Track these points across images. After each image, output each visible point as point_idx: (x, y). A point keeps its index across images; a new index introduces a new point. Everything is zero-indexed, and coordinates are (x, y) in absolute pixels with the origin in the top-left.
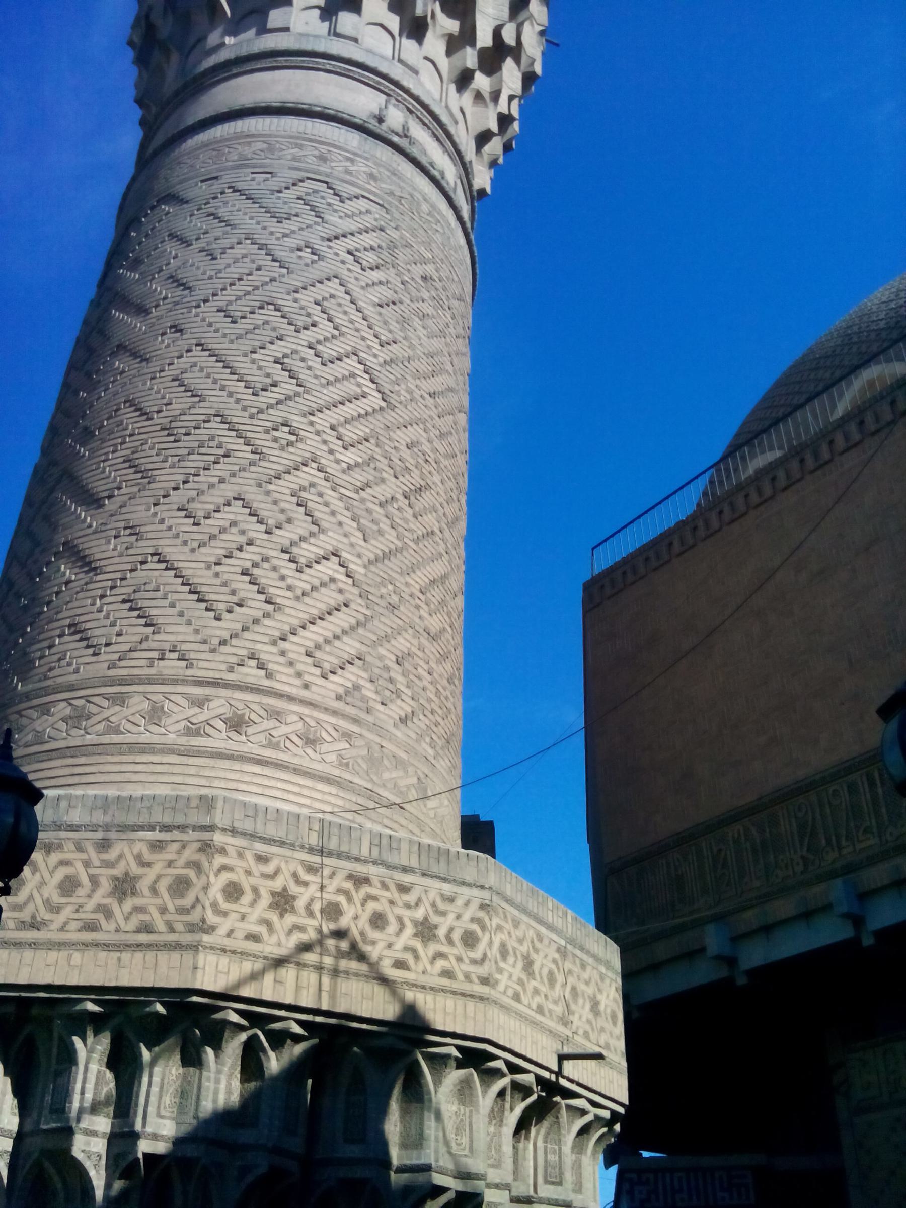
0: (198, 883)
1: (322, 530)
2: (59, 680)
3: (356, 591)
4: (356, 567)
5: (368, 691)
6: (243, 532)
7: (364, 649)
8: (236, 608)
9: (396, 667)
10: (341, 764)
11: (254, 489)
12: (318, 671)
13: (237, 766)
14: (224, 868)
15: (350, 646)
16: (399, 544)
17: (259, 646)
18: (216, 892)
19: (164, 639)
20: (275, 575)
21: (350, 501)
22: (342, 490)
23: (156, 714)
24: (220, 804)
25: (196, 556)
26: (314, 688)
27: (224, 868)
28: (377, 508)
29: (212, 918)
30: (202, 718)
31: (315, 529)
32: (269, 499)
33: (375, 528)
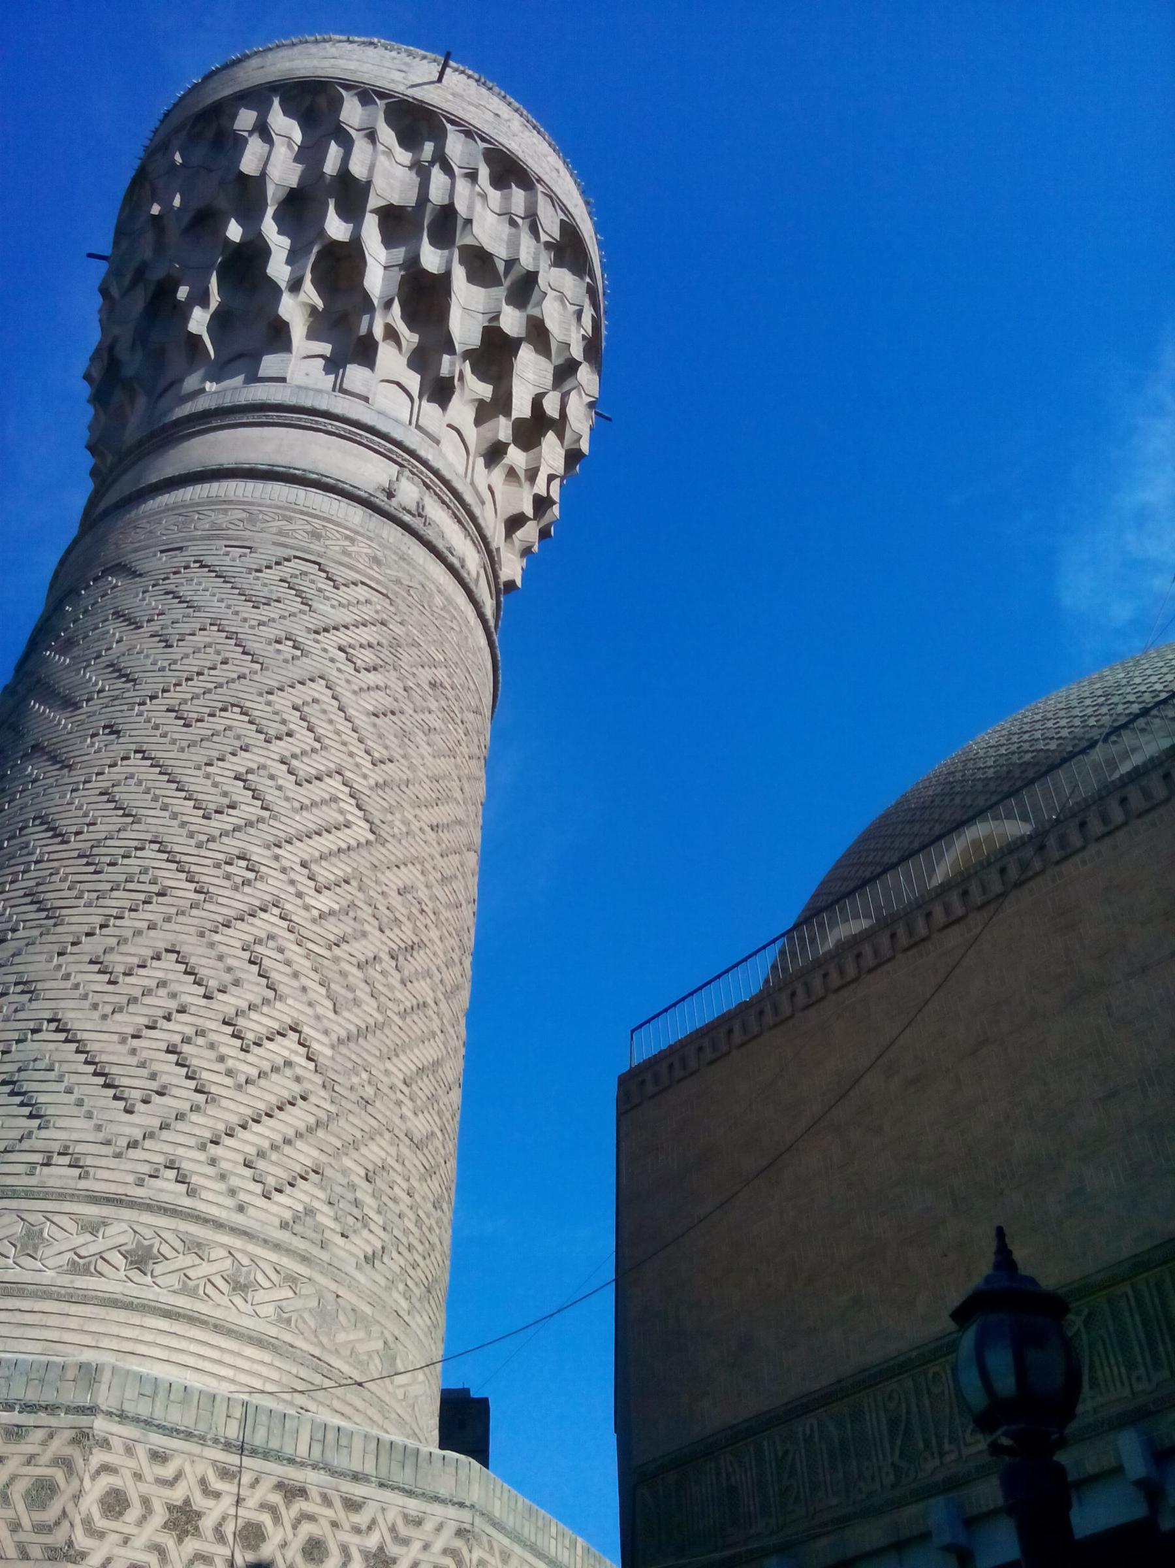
1: (279, 997)
3: (318, 1079)
4: (321, 1048)
5: (325, 1217)
6: (174, 996)
7: (324, 1158)
8: (156, 1098)
9: (365, 1185)
10: (280, 1319)
11: (194, 939)
12: (258, 1188)
13: (136, 1318)
14: (106, 1468)
15: (305, 1154)
16: (380, 1019)
17: (181, 1151)
18: (90, 1503)
19: (54, 1137)
20: (212, 1055)
21: (320, 960)
22: (310, 945)
24: (106, 1376)
25: (109, 1025)
26: (251, 1211)
27: (106, 1468)
28: (354, 970)
29: (82, 1541)
30: (93, 1249)
31: (270, 994)
32: (213, 953)
33: (350, 996)
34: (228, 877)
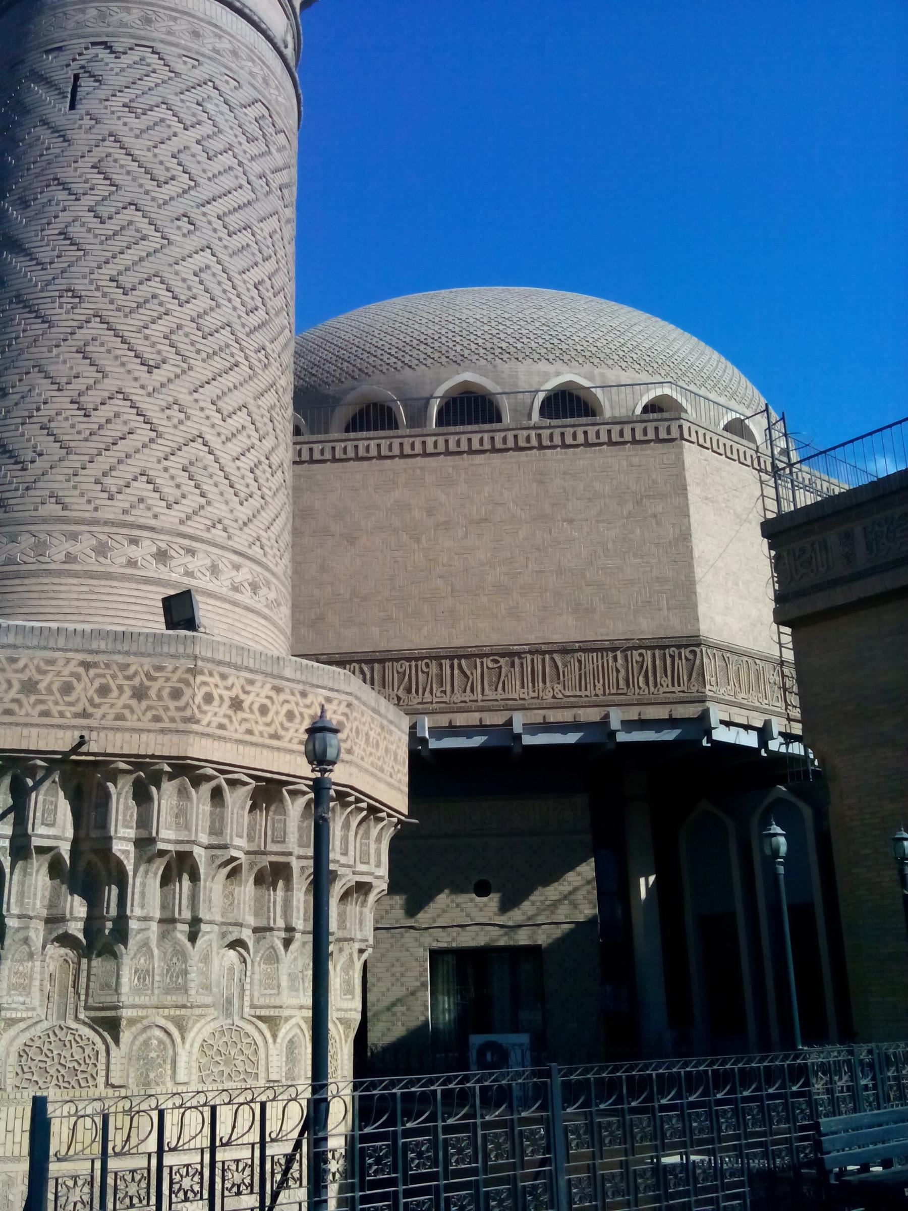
0: (188, 692)
2: (21, 514)
12: (164, 504)
17: (56, 485)
18: (199, 699)
23: (102, 550)
29: (198, 715)
34: (179, 228)
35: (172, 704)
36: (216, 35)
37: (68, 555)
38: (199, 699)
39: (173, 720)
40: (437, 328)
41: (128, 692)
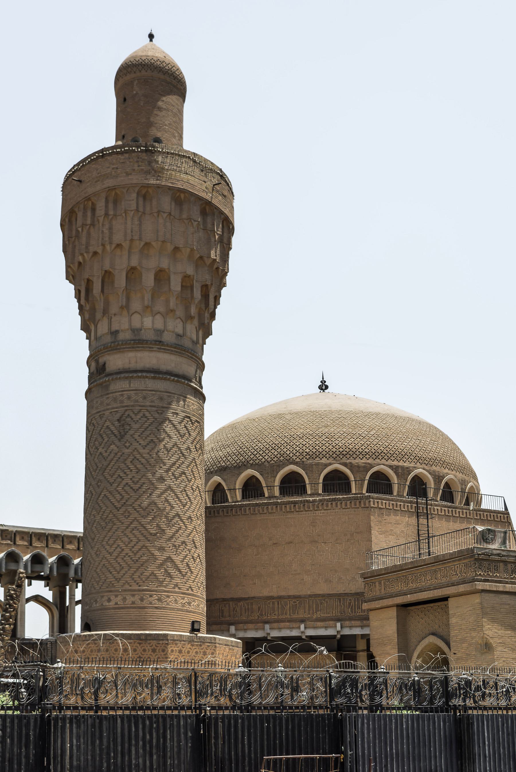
23: (142, 600)
35: (163, 653)
36: (169, 396)
37: (132, 602)
38: (169, 652)
39: (163, 658)
40: (280, 440)
41: (151, 651)
